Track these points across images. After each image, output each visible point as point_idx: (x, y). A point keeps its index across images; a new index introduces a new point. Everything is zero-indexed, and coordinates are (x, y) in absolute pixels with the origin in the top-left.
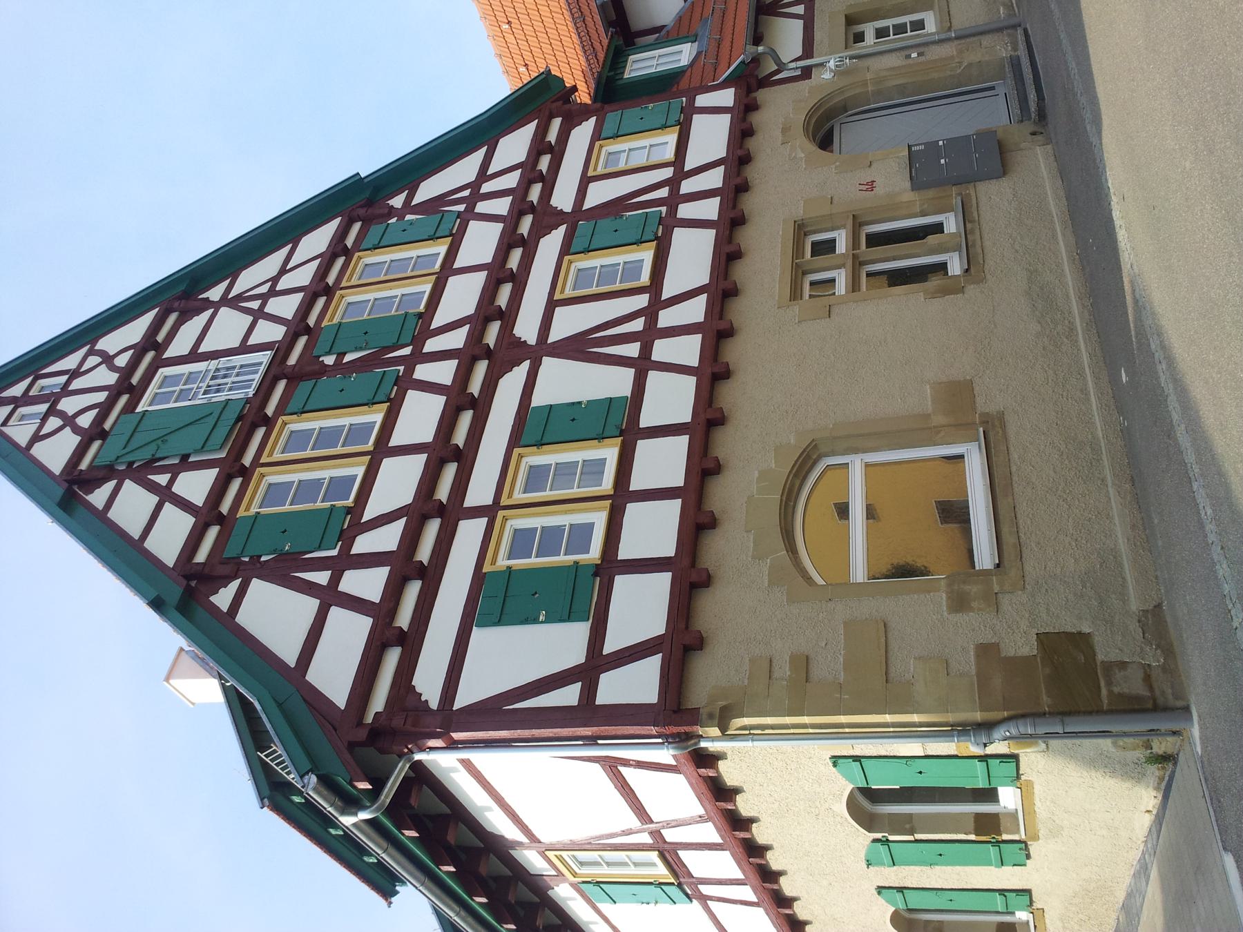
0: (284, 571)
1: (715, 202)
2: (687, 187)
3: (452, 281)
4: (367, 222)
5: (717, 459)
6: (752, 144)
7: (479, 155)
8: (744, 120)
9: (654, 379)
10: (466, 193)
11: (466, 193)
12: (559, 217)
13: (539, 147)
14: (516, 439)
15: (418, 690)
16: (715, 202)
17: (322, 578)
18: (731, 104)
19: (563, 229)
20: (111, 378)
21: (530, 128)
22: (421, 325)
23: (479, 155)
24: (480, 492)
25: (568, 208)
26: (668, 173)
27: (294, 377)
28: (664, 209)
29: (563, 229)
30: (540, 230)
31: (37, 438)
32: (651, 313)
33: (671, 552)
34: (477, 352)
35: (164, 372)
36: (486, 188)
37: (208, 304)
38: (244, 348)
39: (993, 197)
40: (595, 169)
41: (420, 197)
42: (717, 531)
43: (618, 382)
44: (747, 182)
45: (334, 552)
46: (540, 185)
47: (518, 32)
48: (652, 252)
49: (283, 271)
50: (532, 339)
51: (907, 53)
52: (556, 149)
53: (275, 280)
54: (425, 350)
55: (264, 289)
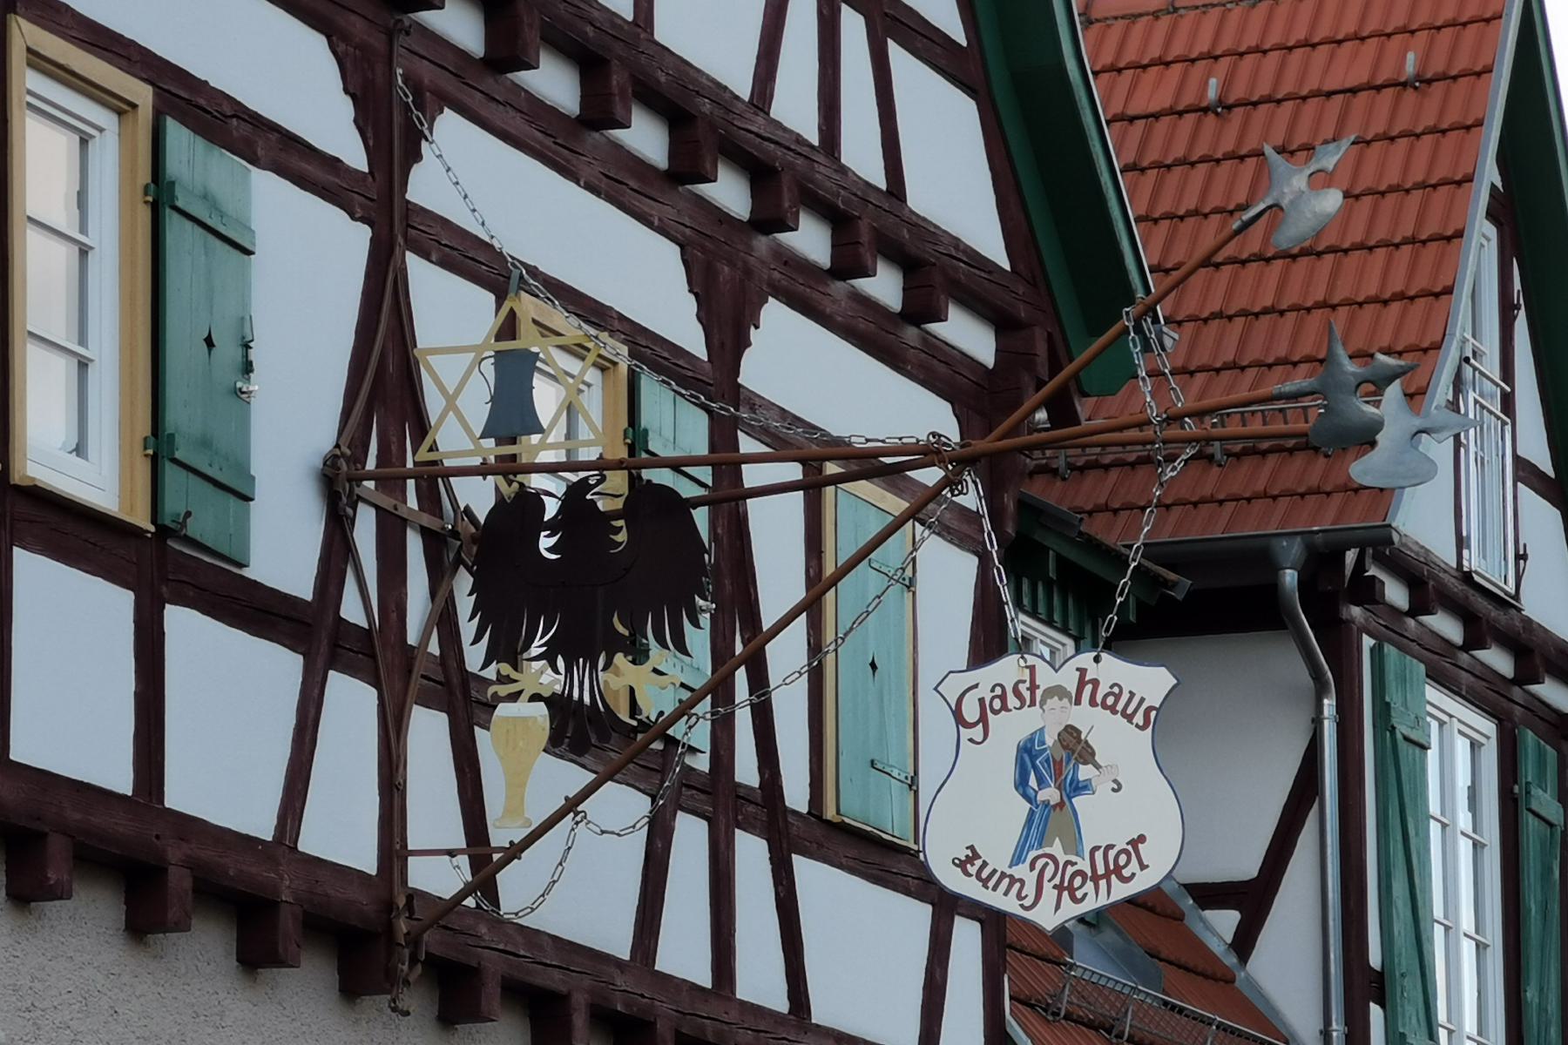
1: (700, 973)
2: (751, 852)
5: (59, 893)
6: (206, 947)
9: (281, 666)
12: (729, 327)
13: (936, 271)
15: (692, 297)
16: (700, 973)
18: (311, 842)
19: (355, 156)
21: (989, 241)
25: (426, 187)
26: (796, 795)
28: (702, 763)
32: (765, 812)
33: (662, 965)
40: (37, 60)
42: (335, 994)
44: (163, 927)
47: (1179, 138)
52: (911, 334)
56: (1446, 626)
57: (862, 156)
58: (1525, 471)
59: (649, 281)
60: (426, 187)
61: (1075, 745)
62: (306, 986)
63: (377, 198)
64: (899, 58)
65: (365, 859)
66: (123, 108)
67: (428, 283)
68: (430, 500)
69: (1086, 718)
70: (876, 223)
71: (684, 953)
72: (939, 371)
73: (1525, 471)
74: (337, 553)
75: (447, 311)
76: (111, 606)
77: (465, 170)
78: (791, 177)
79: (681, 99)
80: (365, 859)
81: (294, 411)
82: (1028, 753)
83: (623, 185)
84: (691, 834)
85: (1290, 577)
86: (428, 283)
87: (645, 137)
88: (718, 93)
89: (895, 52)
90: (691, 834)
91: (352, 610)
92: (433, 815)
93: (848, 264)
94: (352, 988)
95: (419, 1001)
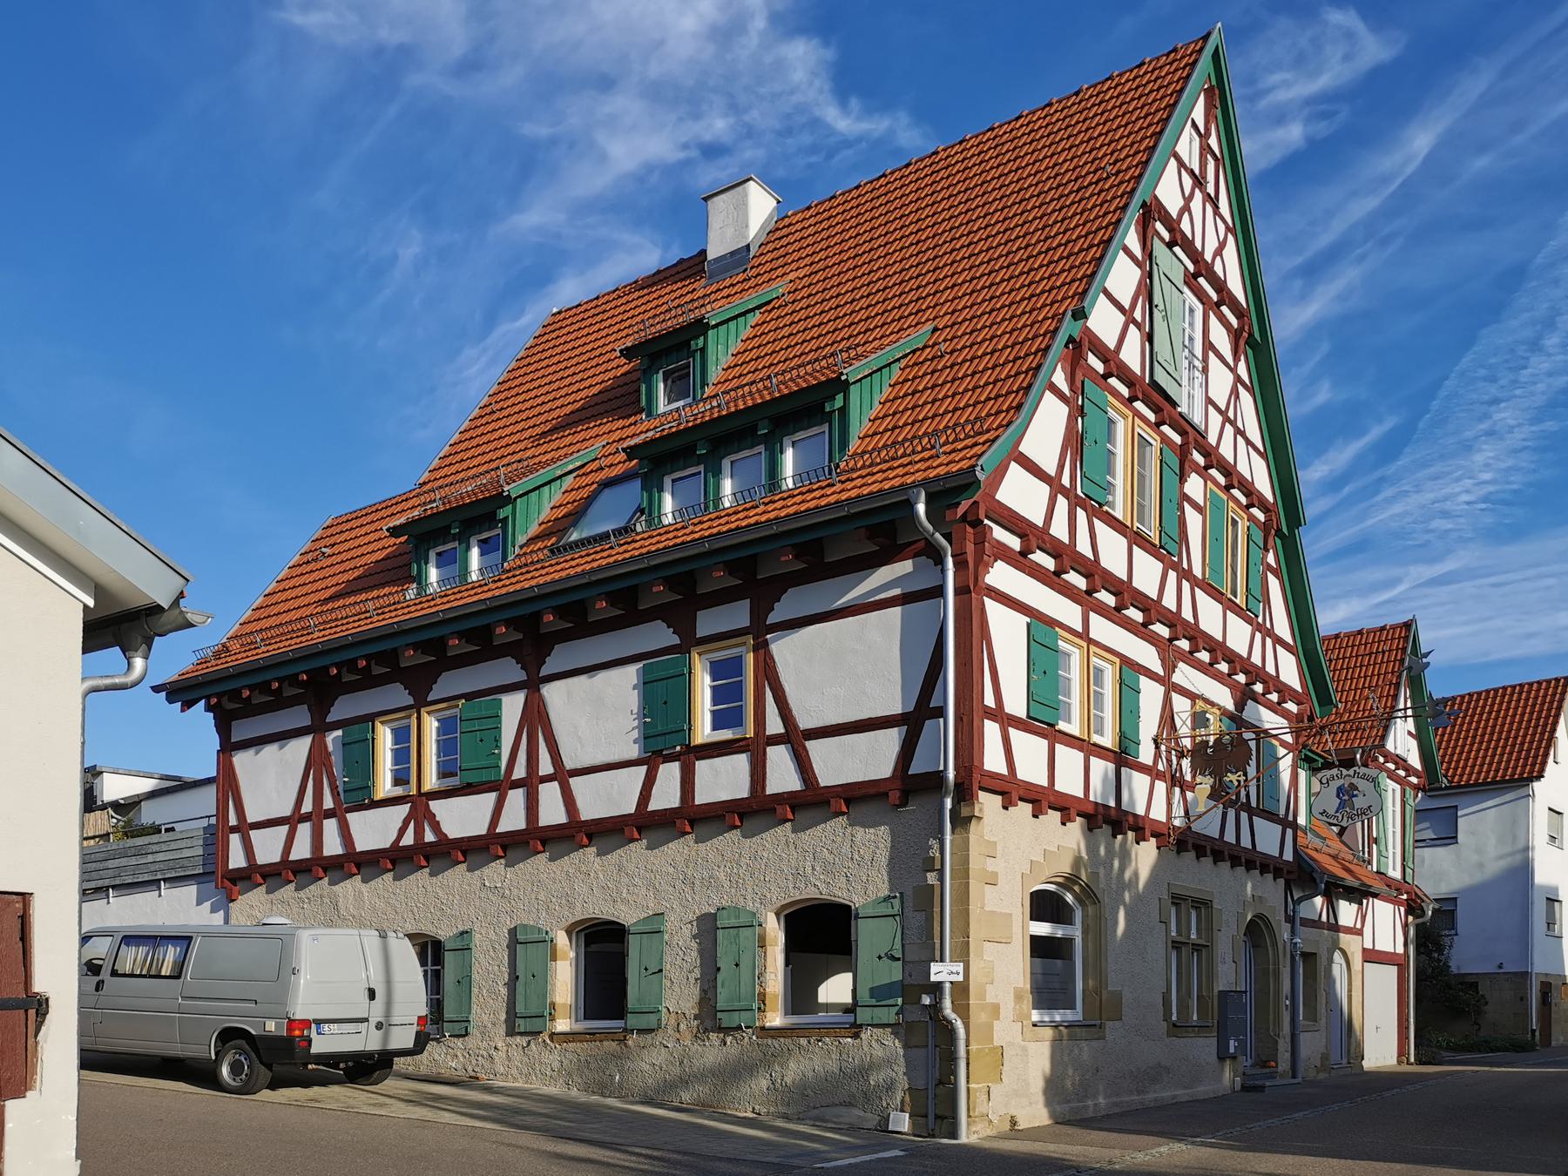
0: (1075, 443)
2: (1244, 816)
3: (1123, 542)
4: (1265, 528)
7: (1288, 639)
8: (1155, 835)
9: (1146, 779)
10: (1185, 566)
11: (1185, 566)
14: (1126, 662)
17: (1066, 481)
18: (1060, 786)
19: (1161, 673)
20: (1208, 257)
21: (1296, 685)
22: (1098, 511)
23: (1288, 639)
24: (1102, 629)
26: (1254, 804)
27: (1183, 453)
29: (1161, 673)
30: (1233, 687)
31: (1181, 164)
32: (1247, 806)
34: (1066, 561)
35: (1199, 308)
36: (1269, 641)
37: (1236, 359)
38: (1209, 401)
39: (1205, 1047)
41: (1271, 577)
43: (1146, 754)
45: (1079, 492)
46: (1052, 568)
48: (1077, 734)
49: (1249, 442)
50: (1177, 678)
51: (227, 929)
53: (1242, 433)
54: (1060, 497)
55: (1240, 424)
56: (1391, 766)
57: (1270, 669)
58: (1410, 733)
59: (1223, 697)
60: (1177, 678)
61: (1353, 787)
62: (1207, 861)
63: (1171, 688)
64: (1278, 648)
65: (1163, 819)
66: (1112, 663)
67: (1176, 697)
68: (1177, 744)
69: (1355, 781)
70: (1273, 683)
71: (1230, 837)
72: (1285, 714)
73: (1410, 733)
74: (1157, 755)
75: (1181, 704)
76: (1078, 756)
77: (1185, 675)
78: (1256, 674)
79: (1232, 658)
80: (1163, 819)
81: (1148, 726)
82: (1340, 790)
83: (1218, 676)
84: (1231, 813)
85: (921, 508)
86: (1176, 697)
87: (1204, 656)
88: (1240, 657)
89: (1096, 521)
90: (1231, 813)
91: (1160, 767)
92: (1178, 811)
93: (1267, 691)
94: (1248, 870)
95: (1192, 855)
